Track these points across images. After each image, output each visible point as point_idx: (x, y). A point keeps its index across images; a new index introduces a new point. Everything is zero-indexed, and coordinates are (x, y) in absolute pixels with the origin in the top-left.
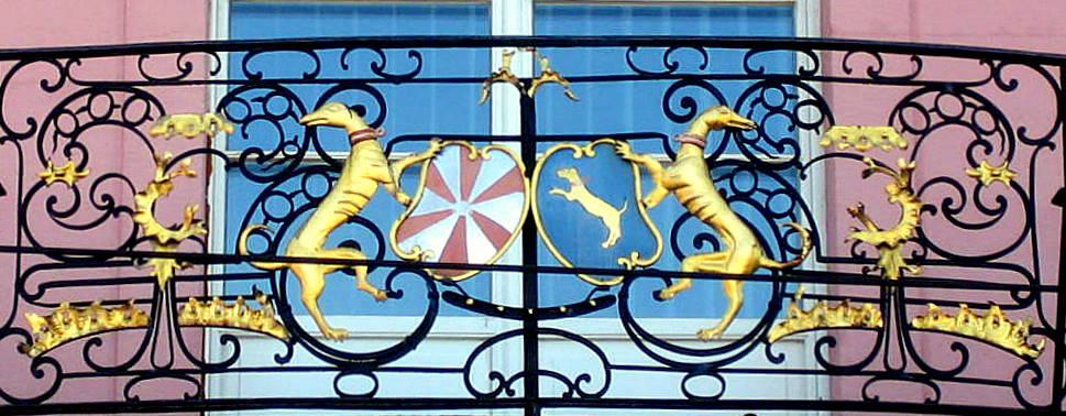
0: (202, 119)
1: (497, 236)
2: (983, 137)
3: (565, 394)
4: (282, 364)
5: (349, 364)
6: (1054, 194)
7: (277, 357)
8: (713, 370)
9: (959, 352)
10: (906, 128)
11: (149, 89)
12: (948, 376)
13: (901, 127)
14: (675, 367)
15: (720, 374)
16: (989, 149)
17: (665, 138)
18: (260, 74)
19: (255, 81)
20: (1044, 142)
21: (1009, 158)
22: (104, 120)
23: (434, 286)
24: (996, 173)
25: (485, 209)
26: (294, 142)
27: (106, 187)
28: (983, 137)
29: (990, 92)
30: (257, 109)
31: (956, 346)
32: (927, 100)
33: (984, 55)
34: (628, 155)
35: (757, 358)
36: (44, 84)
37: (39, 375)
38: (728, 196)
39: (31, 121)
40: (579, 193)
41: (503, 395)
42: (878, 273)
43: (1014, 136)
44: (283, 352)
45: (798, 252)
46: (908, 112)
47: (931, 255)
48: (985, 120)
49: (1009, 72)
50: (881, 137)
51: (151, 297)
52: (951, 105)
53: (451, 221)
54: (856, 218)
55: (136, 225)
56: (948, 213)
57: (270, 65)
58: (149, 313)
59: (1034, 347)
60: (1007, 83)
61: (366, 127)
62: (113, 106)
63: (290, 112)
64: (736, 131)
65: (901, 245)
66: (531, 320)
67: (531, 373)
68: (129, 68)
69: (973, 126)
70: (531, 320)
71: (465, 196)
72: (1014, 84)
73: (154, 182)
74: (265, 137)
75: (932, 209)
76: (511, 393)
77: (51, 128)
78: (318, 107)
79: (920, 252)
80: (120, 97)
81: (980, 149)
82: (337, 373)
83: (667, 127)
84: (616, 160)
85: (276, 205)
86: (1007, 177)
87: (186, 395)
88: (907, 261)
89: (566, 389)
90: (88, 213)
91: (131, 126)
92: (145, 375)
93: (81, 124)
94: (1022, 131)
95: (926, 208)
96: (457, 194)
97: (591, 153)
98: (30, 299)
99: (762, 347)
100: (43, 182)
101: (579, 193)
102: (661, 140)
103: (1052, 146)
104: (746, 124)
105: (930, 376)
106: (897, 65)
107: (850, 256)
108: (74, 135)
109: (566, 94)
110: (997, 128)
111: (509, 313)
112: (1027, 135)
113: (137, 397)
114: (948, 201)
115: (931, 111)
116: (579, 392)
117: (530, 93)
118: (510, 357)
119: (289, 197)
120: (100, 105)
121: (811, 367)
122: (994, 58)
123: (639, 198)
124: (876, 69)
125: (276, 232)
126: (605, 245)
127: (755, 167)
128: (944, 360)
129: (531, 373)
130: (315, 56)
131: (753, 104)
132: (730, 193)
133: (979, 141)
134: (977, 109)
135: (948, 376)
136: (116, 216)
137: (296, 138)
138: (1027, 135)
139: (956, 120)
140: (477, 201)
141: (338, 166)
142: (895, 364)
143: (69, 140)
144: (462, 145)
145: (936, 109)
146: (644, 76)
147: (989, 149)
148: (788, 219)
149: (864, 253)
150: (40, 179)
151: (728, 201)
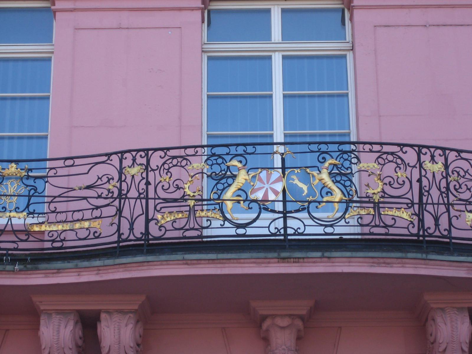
2: (399, 165)
3: (294, 233)
5: (239, 226)
7: (221, 225)
8: (331, 226)
9: (394, 220)
10: (379, 163)
12: (391, 226)
13: (378, 163)
14: (321, 225)
16: (400, 169)
17: (318, 167)
19: (214, 155)
22: (176, 165)
26: (224, 170)
27: (177, 182)
28: (399, 165)
29: (400, 154)
30: (215, 162)
31: (393, 219)
32: (384, 156)
33: (398, 145)
35: (342, 222)
36: (160, 157)
37: (161, 230)
38: (334, 182)
39: (157, 166)
40: (297, 182)
41: (278, 233)
42: (373, 200)
44: (222, 223)
46: (440, 152)
47: (386, 196)
48: (399, 161)
49: (405, 149)
50: (373, 166)
51: (188, 210)
52: (390, 158)
55: (185, 192)
56: (390, 185)
60: (405, 152)
62: (178, 162)
63: (223, 162)
65: (378, 193)
66: (285, 214)
67: (285, 227)
68: (182, 152)
69: (396, 163)
70: (285, 214)
73: (189, 181)
75: (386, 184)
76: (280, 233)
77: (162, 168)
79: (383, 195)
83: (318, 164)
85: (220, 186)
90: (172, 189)
92: (187, 230)
93: (170, 167)
94: (408, 164)
96: (266, 182)
97: (299, 172)
98: (158, 211)
100: (161, 182)
103: (416, 168)
104: (338, 163)
105: (386, 226)
106: (376, 148)
108: (168, 169)
110: (402, 163)
111: (279, 212)
115: (386, 159)
116: (298, 232)
117: (284, 156)
119: (223, 184)
120: (175, 162)
123: (312, 182)
124: (371, 149)
125: (220, 193)
126: (303, 195)
127: (341, 174)
128: (390, 222)
129: (285, 227)
131: (340, 158)
132: (335, 181)
133: (398, 167)
134: (397, 158)
135: (391, 226)
136: (179, 190)
137: (225, 169)
139: (392, 161)
142: (377, 223)
143: (167, 171)
144: (267, 170)
145: (387, 159)
147: (400, 169)
149: (369, 195)
150: (160, 181)
151: (334, 183)
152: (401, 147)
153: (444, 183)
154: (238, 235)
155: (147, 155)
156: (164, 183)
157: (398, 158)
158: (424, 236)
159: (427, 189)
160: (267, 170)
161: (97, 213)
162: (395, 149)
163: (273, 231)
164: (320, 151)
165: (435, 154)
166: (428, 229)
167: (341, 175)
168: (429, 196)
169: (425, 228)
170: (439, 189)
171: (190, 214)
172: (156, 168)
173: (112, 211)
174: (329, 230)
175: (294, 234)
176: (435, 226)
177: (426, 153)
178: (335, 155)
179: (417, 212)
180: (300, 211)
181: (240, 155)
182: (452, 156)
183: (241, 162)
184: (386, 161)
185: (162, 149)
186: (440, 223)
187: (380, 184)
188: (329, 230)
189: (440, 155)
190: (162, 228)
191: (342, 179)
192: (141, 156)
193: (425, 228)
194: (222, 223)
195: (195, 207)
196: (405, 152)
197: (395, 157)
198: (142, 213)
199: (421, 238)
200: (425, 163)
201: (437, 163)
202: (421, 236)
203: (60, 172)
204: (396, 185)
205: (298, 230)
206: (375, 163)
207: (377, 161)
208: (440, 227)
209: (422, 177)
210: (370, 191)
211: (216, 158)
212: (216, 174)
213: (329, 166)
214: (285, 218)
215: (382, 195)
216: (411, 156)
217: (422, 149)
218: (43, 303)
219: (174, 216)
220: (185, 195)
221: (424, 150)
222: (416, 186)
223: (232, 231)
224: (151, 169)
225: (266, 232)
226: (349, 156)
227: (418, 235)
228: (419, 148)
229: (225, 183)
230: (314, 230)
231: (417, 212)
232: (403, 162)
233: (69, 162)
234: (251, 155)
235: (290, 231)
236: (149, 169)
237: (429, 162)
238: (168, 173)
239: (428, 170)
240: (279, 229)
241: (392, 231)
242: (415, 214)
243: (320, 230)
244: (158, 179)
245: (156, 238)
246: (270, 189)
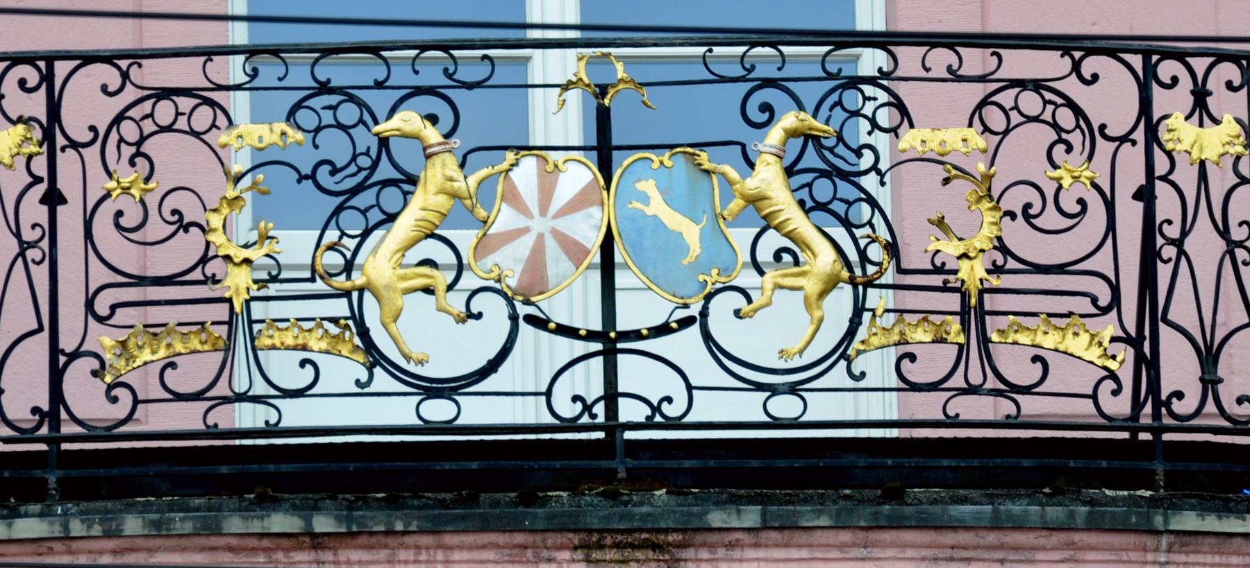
0: (271, 130)
1: (575, 252)
2: (1064, 136)
3: (648, 418)
4: (363, 389)
6: (1134, 190)
7: (358, 382)
8: (793, 389)
9: (1039, 365)
10: (986, 129)
11: (216, 96)
12: (1027, 390)
13: (982, 128)
14: (760, 387)
15: (802, 393)
16: (1069, 149)
17: (743, 146)
18: (329, 81)
19: (324, 88)
20: (1123, 139)
21: (1090, 158)
22: (169, 129)
23: (513, 307)
24: (1076, 174)
25: (563, 225)
26: (367, 153)
27: (172, 202)
28: (1064, 136)
29: (1072, 87)
30: (327, 117)
31: (1036, 359)
32: (1006, 98)
33: (1062, 43)
34: (707, 165)
35: (838, 377)
36: (104, 88)
37: (114, 400)
38: (807, 207)
39: (93, 128)
40: (657, 207)
41: (585, 419)
42: (958, 285)
43: (1094, 133)
44: (364, 377)
45: (879, 264)
47: (1012, 264)
48: (1066, 118)
49: (1091, 65)
50: (961, 140)
51: (226, 319)
52: (1031, 102)
53: (527, 242)
55: (208, 244)
56: (1028, 218)
57: (338, 72)
58: (225, 337)
59: (1114, 357)
60: (1089, 78)
61: (442, 140)
62: (178, 114)
63: (361, 121)
64: (816, 139)
65: (981, 254)
66: (610, 342)
67: (611, 396)
68: (185, 73)
69: (1055, 125)
70: (610, 342)
71: (544, 211)
72: (1095, 77)
73: (225, 198)
74: (336, 147)
75: (1012, 216)
76: (594, 416)
77: (114, 136)
78: (393, 111)
79: (1000, 262)
80: (186, 103)
81: (1061, 148)
82: (419, 398)
83: (742, 132)
84: (694, 170)
85: (353, 222)
86: (1087, 178)
87: (267, 422)
88: (989, 272)
89: (648, 412)
90: (156, 229)
91: (197, 135)
92: (225, 400)
93: (146, 133)
94: (1103, 127)
95: (1007, 213)
96: (535, 209)
97: (668, 163)
98: (101, 320)
99: (843, 364)
100: (108, 195)
101: (657, 207)
102: (739, 147)
103: (1134, 143)
104: (825, 132)
105: (1012, 390)
106: (975, 60)
107: (931, 267)
108: (139, 144)
109: (644, 102)
110: (1078, 126)
111: (591, 336)
112: (1107, 132)
113: (216, 425)
114: (1028, 206)
115: (1011, 109)
116: (663, 415)
117: (606, 102)
119: (364, 212)
120: (165, 112)
121: (894, 385)
123: (718, 210)
124: (955, 67)
125: (352, 248)
126: (685, 262)
127: (832, 173)
128: (1025, 374)
129: (611, 396)
130: (456, 402)
131: (831, 109)
132: (809, 204)
133: (1060, 141)
134: (1057, 106)
135: (1027, 390)
136: (186, 231)
137: (369, 148)
138: (1107, 132)
139: (1036, 119)
140: (555, 216)
141: (413, 180)
142: (976, 378)
143: (133, 150)
144: (537, 156)
145: (1016, 108)
146: (723, 80)
147: (1069, 149)
148: (867, 230)
149: (944, 264)
150: (105, 192)
151: (807, 212)
152: (1072, 57)
154: (429, 427)
155: (47, 78)
156: (124, 203)
157: (1062, 105)
158: (1157, 430)
159: (1173, 232)
160: (537, 156)
162: (1050, 64)
163: (568, 410)
164: (751, 76)
165: (1210, 86)
166: (1174, 400)
167: (827, 173)
168: (1183, 260)
169: (1164, 397)
170: (1224, 233)
171: (231, 336)
172: (88, 136)
174: (786, 407)
175: (648, 425)
176: (1200, 385)
177: (1175, 80)
178: (810, 93)
179: (1132, 331)
180: (673, 331)
181: (431, 91)
183: (433, 119)
184: (1015, 118)
185: (108, 58)
186: (1221, 372)
187: (990, 217)
188: (786, 407)
189: (1229, 86)
190: (117, 392)
191: (838, 196)
192: (22, 83)
193: (1164, 397)
194: (364, 377)
195: (253, 304)
196: (1089, 78)
197: (1051, 102)
198: (35, 326)
199: (1144, 436)
200: (1167, 121)
201: (1217, 122)
202: (1145, 429)
205: (665, 407)
206: (970, 125)
207: (977, 116)
208: (1221, 388)
209: (1157, 182)
210: (951, 249)
211: (333, 99)
212: (334, 171)
213: (784, 144)
214: (610, 356)
215: (994, 263)
216: (1111, 95)
217: (1159, 61)
219: (169, 346)
220: (211, 254)
221: (1168, 69)
222: (1130, 215)
223: (400, 411)
224: (66, 143)
225: (531, 412)
226: (866, 99)
227: (1131, 422)
228: (1149, 55)
229: (372, 207)
230: (728, 409)
231: (1133, 332)
232: (1082, 123)
234: (476, 90)
235: (629, 411)
236: (60, 141)
237: (1187, 118)
238: (138, 160)
239: (1179, 152)
240: (589, 403)
241: (1031, 406)
242: (1127, 340)
243: (749, 407)
244: (99, 184)
246: (527, 208)
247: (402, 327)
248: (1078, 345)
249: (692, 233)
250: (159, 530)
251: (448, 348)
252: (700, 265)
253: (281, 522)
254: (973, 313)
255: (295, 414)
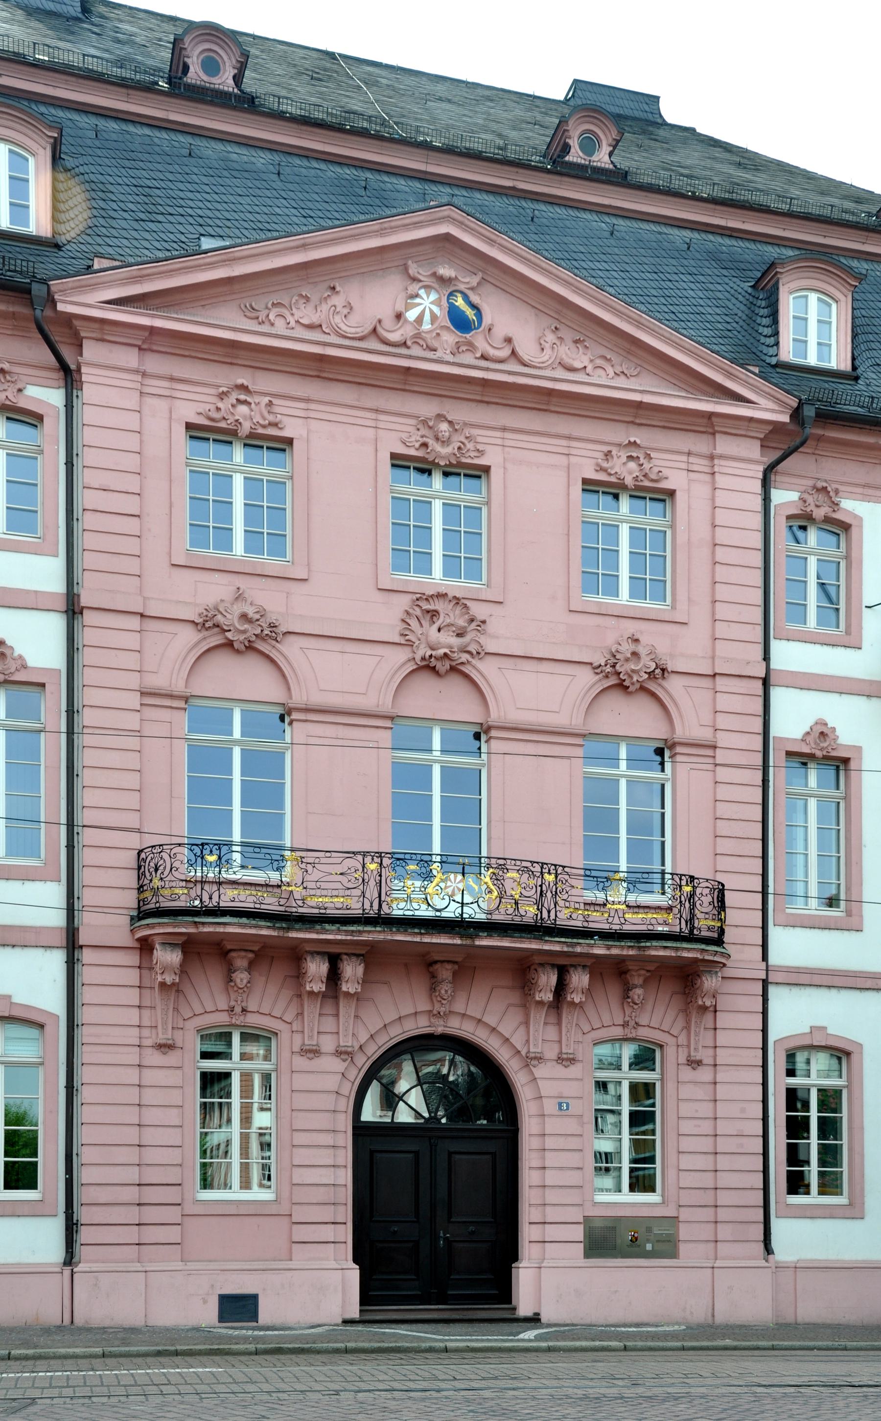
5: (438, 910)
19: (422, 861)
29: (531, 868)
33: (353, 853)
40: (471, 883)
46: (553, 867)
49: (535, 865)
54: (808, 1030)
68: (402, 856)
74: (424, 870)
101: (471, 883)
106: (518, 863)
118: (459, 910)
122: (532, 862)
127: (497, 879)
128: (523, 914)
153: (554, 889)
161: (348, 892)
173: (358, 892)
182: (560, 870)
203: (323, 861)
204: (528, 889)
210: (514, 893)
214: (462, 907)
218: (631, 966)
221: (545, 866)
222: (539, 888)
225: (452, 915)
230: (481, 917)
233: (328, 854)
243: (483, 916)
244: (388, 874)
245: (386, 914)
247: (434, 900)
248: (531, 909)
249: (476, 888)
250: (398, 930)
251: (440, 904)
252: (478, 893)
253: (416, 931)
254: (516, 903)
255: (417, 913)
